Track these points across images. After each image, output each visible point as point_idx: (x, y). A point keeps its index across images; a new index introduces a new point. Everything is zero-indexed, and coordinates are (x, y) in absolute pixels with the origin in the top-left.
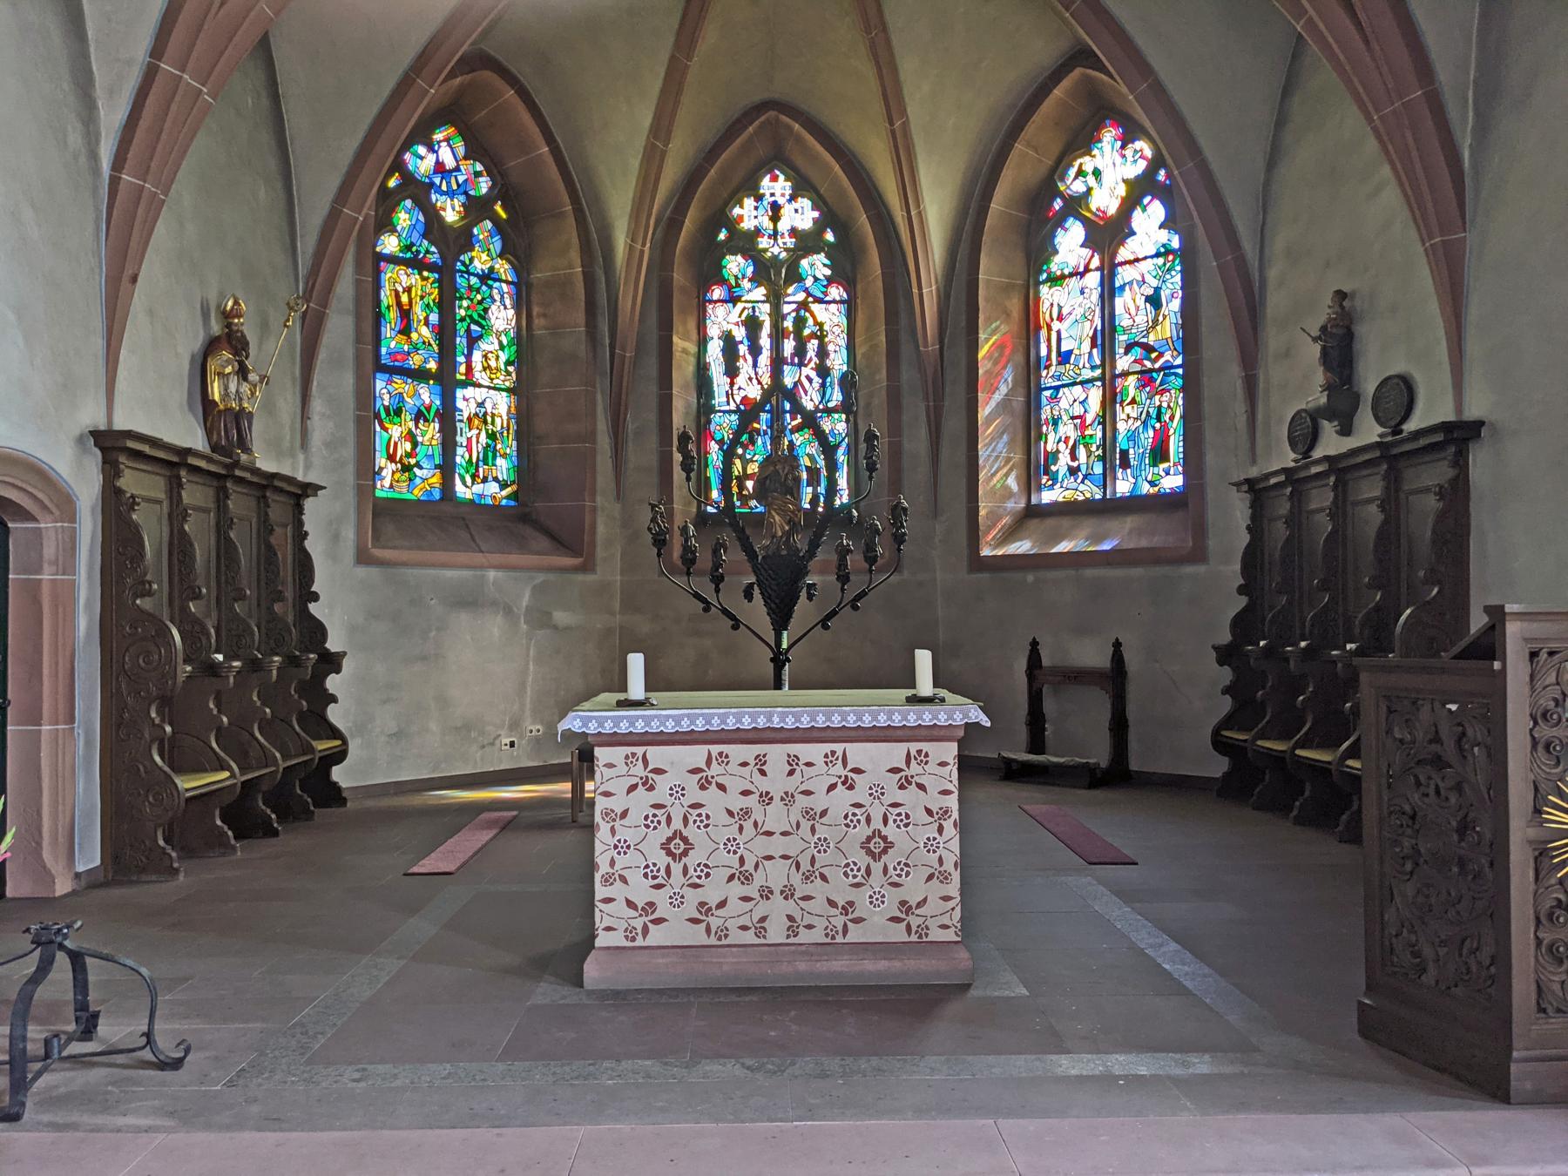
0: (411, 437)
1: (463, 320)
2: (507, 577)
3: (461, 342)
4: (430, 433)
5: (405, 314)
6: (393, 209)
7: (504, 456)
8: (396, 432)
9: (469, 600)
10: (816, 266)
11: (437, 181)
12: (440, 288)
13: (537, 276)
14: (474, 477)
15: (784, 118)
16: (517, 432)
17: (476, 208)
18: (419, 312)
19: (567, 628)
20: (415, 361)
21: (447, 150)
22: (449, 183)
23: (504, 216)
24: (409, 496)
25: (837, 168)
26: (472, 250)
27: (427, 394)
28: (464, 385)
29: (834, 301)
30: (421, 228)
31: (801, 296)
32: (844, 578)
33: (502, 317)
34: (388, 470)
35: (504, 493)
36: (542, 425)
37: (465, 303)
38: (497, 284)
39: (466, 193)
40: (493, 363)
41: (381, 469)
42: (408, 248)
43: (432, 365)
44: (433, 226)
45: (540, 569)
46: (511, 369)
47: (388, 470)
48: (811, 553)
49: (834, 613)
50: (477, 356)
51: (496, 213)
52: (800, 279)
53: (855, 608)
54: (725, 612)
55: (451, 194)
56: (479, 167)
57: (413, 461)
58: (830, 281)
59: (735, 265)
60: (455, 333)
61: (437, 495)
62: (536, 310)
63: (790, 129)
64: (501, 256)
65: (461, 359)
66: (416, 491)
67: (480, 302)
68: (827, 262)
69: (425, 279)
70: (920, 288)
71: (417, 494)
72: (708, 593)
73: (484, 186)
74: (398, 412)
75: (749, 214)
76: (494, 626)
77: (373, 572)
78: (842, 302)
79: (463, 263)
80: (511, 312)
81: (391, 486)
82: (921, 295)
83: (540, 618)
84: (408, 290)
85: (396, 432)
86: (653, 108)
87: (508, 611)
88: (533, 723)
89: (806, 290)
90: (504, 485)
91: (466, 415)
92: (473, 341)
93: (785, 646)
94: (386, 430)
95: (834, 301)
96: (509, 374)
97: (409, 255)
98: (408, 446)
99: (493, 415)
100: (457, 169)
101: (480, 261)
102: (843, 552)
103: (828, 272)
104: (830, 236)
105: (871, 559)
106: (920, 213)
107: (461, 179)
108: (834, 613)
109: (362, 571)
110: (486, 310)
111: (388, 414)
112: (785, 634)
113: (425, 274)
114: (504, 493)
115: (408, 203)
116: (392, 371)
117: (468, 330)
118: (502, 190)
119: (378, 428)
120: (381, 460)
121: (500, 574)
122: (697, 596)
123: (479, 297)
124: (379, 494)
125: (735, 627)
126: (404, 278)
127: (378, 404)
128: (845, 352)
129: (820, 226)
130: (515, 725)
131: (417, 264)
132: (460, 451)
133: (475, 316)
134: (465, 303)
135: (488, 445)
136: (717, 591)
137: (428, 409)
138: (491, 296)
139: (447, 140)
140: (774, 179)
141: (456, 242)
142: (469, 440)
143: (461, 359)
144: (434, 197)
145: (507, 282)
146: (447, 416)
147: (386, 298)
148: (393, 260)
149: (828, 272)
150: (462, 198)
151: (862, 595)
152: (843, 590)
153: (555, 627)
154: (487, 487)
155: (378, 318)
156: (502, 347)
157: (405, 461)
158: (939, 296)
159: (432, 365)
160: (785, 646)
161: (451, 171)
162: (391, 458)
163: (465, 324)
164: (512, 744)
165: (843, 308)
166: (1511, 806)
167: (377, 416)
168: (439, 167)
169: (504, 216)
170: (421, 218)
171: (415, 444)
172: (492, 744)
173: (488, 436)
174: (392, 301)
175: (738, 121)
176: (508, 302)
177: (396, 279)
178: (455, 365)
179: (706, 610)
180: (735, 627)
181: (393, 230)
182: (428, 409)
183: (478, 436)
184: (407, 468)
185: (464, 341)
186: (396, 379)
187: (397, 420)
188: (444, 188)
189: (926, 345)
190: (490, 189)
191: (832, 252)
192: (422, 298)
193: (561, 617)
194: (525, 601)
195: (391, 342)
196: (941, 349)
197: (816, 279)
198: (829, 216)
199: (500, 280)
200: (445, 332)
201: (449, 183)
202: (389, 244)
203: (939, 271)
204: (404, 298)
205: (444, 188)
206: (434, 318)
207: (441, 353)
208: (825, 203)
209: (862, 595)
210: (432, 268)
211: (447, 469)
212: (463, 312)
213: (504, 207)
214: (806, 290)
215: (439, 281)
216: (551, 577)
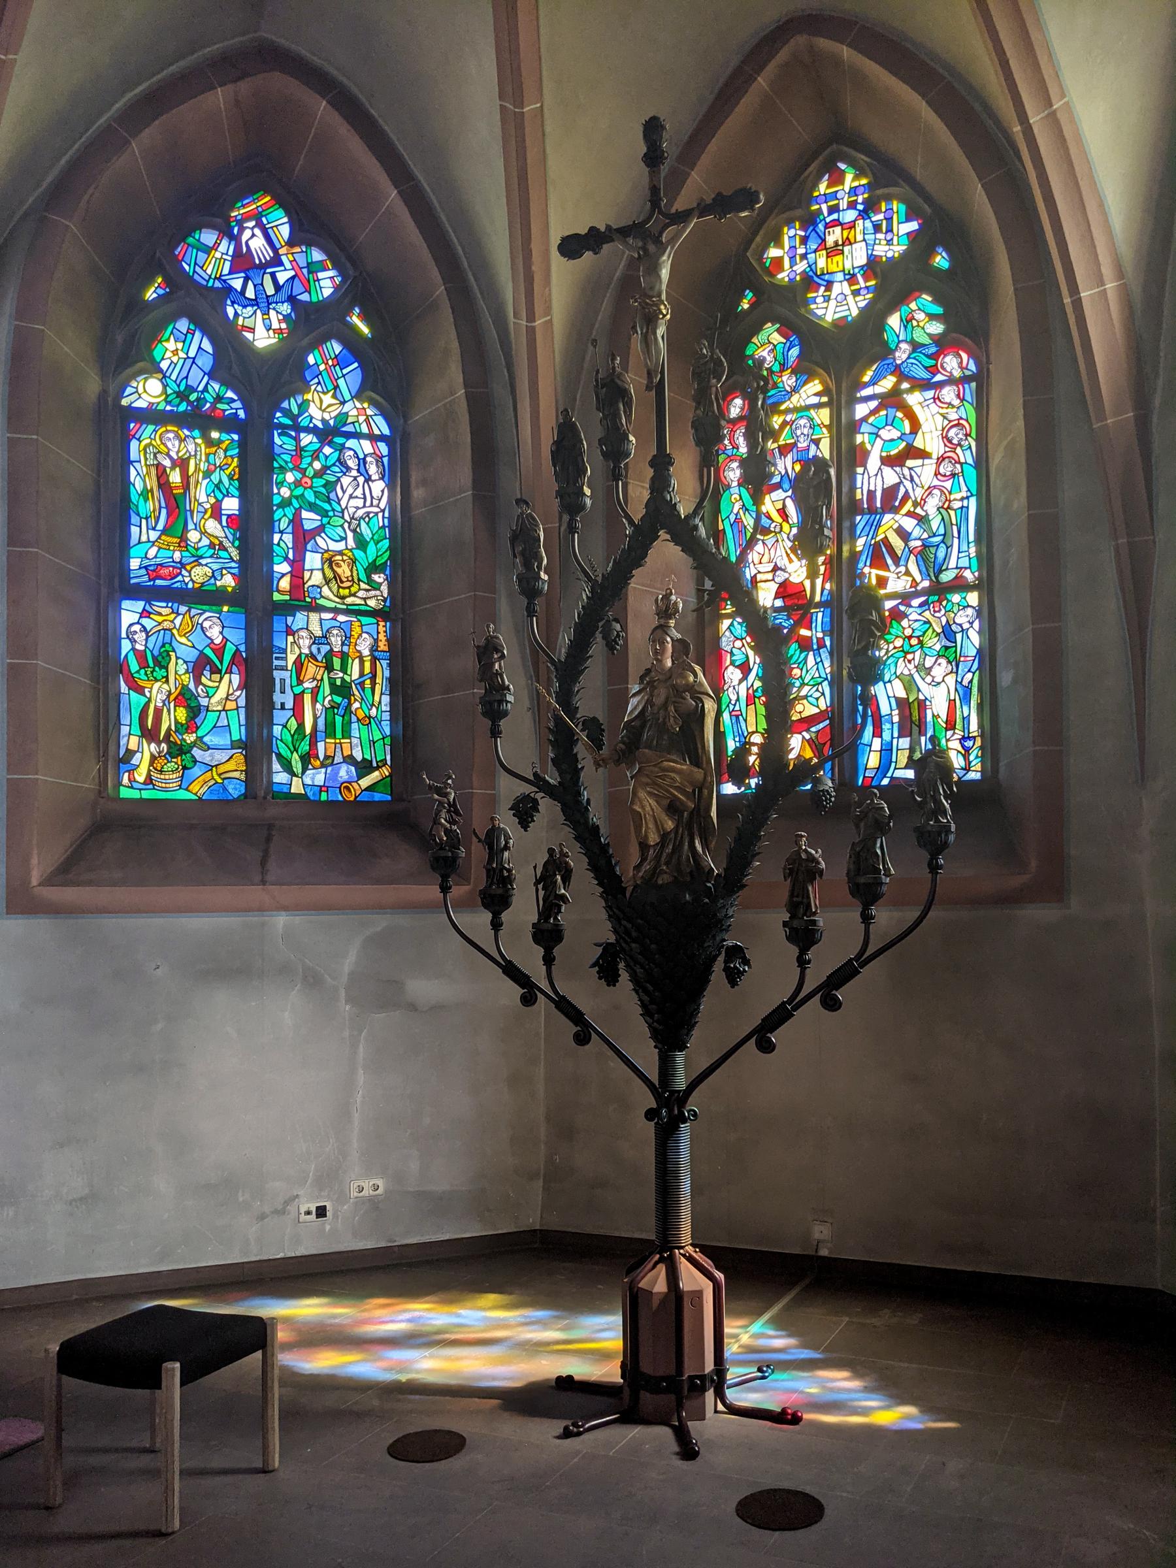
0: (184, 698)
1: (286, 503)
2: (315, 930)
3: (284, 541)
4: (224, 690)
5: (175, 503)
6: (155, 337)
7: (367, 721)
8: (158, 693)
9: (233, 968)
10: (919, 321)
11: (237, 284)
12: (242, 457)
13: (419, 416)
14: (306, 760)
15: (823, 43)
16: (391, 681)
17: (312, 323)
18: (202, 494)
19: (437, 1008)
20: (198, 575)
21: (265, 228)
22: (259, 287)
23: (365, 329)
24: (183, 795)
25: (927, 114)
26: (307, 389)
27: (217, 628)
28: (288, 609)
29: (951, 381)
30: (206, 362)
31: (888, 383)
32: (803, 936)
33: (366, 497)
34: (145, 754)
35: (365, 782)
36: (425, 664)
37: (290, 477)
38: (352, 443)
39: (292, 299)
40: (344, 570)
41: (130, 753)
42: (182, 396)
43: (228, 581)
44: (232, 360)
45: (379, 907)
46: (378, 578)
47: (145, 754)
48: (732, 881)
49: (780, 1016)
50: (312, 560)
51: (353, 328)
52: (884, 352)
53: (831, 1004)
54: (564, 1006)
55: (263, 303)
56: (317, 255)
57: (190, 738)
58: (942, 345)
59: (769, 345)
60: (269, 525)
61: (235, 790)
62: (414, 477)
63: (837, 62)
64: (358, 396)
65: (282, 568)
66: (195, 787)
67: (319, 474)
68: (938, 310)
69: (210, 443)
70: (1074, 289)
71: (198, 789)
72: (531, 961)
73: (326, 284)
74: (161, 662)
75: (787, 256)
76: (286, 1010)
77: (39, 928)
78: (965, 380)
79: (287, 413)
80: (378, 487)
81: (149, 780)
82: (1078, 304)
83: (381, 992)
84: (182, 464)
85: (158, 693)
86: (492, 40)
87: (313, 981)
88: (368, 1174)
89: (897, 371)
90: (365, 767)
91: (291, 658)
92: (303, 538)
93: (681, 1083)
94: (140, 690)
95: (951, 381)
96: (376, 587)
97: (183, 407)
98: (182, 714)
99: (344, 656)
100: (277, 261)
101: (319, 407)
102: (802, 873)
103: (937, 328)
104: (941, 261)
105: (866, 891)
106: (1053, 120)
107: (282, 277)
108: (780, 1016)
109: (17, 926)
110: (330, 486)
111: (143, 663)
112: (680, 1058)
113: (215, 435)
114: (365, 782)
115: (183, 325)
116: (148, 594)
117: (296, 522)
118: (360, 288)
119: (124, 688)
120: (130, 738)
121: (297, 920)
122: (511, 971)
123: (317, 465)
124: (125, 793)
125: (582, 1039)
126: (173, 446)
127: (126, 646)
128: (971, 473)
129: (922, 245)
130: (329, 1178)
131: (197, 418)
132: (279, 717)
133: (310, 496)
134: (290, 477)
135: (334, 706)
136: (549, 960)
137: (220, 651)
138: (341, 462)
139: (257, 217)
140: (837, 178)
141: (261, 389)
142: (298, 699)
143: (282, 568)
144: (230, 311)
145: (373, 438)
146: (257, 670)
147: (139, 479)
148: (152, 416)
149: (937, 328)
150: (286, 308)
151: (845, 974)
152: (802, 963)
153: (413, 1007)
154: (342, 751)
155: (122, 511)
156: (361, 544)
157: (175, 738)
158: (1125, 292)
159: (228, 581)
160: (681, 1083)
161: (263, 267)
162: (150, 734)
163: (290, 512)
164: (321, 1212)
165: (970, 390)
166: (1059, 208)
167: (123, 668)
168: (243, 262)
169: (365, 329)
170: (207, 345)
171: (195, 712)
172: (282, 1212)
173: (334, 689)
174: (152, 483)
175: (738, 72)
176: (373, 469)
177: (149, 448)
178: (269, 580)
179: (528, 1000)
180: (582, 1039)
181: (154, 369)
182: (220, 651)
183: (315, 692)
184: (178, 750)
185: (288, 538)
186: (160, 606)
187: (160, 673)
188: (250, 293)
189: (1102, 417)
190: (337, 288)
191: (944, 289)
192: (208, 474)
193: (423, 988)
194: (348, 963)
195: (146, 547)
196: (1143, 423)
197: (916, 346)
198: (940, 225)
199: (357, 435)
200: (252, 529)
201: (259, 287)
202: (147, 392)
203: (1126, 251)
204: (175, 477)
205: (250, 293)
206: (231, 505)
207: (243, 562)
208: (928, 199)
209: (845, 974)
210: (229, 424)
211: (256, 748)
212: (285, 492)
213: (364, 317)
214: (897, 371)
215: (242, 445)
216: (403, 920)
